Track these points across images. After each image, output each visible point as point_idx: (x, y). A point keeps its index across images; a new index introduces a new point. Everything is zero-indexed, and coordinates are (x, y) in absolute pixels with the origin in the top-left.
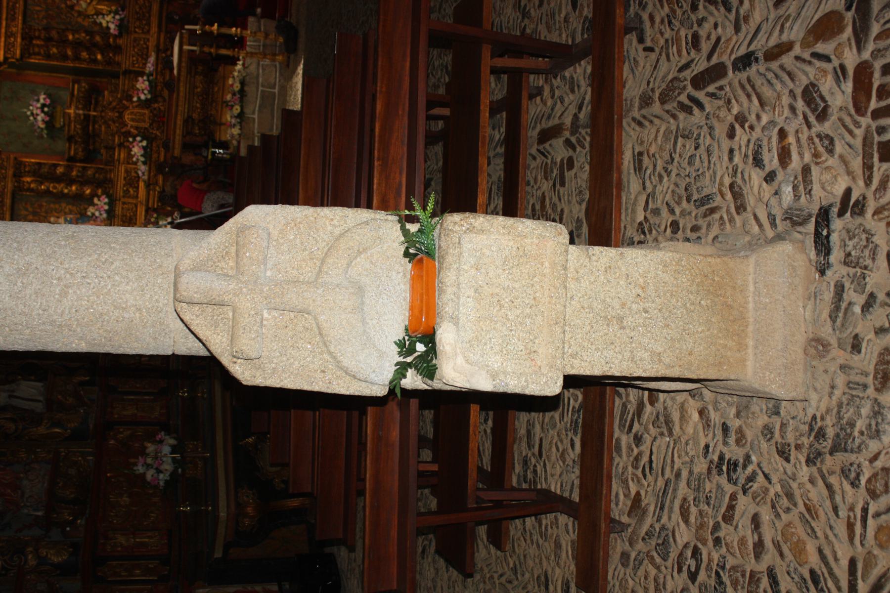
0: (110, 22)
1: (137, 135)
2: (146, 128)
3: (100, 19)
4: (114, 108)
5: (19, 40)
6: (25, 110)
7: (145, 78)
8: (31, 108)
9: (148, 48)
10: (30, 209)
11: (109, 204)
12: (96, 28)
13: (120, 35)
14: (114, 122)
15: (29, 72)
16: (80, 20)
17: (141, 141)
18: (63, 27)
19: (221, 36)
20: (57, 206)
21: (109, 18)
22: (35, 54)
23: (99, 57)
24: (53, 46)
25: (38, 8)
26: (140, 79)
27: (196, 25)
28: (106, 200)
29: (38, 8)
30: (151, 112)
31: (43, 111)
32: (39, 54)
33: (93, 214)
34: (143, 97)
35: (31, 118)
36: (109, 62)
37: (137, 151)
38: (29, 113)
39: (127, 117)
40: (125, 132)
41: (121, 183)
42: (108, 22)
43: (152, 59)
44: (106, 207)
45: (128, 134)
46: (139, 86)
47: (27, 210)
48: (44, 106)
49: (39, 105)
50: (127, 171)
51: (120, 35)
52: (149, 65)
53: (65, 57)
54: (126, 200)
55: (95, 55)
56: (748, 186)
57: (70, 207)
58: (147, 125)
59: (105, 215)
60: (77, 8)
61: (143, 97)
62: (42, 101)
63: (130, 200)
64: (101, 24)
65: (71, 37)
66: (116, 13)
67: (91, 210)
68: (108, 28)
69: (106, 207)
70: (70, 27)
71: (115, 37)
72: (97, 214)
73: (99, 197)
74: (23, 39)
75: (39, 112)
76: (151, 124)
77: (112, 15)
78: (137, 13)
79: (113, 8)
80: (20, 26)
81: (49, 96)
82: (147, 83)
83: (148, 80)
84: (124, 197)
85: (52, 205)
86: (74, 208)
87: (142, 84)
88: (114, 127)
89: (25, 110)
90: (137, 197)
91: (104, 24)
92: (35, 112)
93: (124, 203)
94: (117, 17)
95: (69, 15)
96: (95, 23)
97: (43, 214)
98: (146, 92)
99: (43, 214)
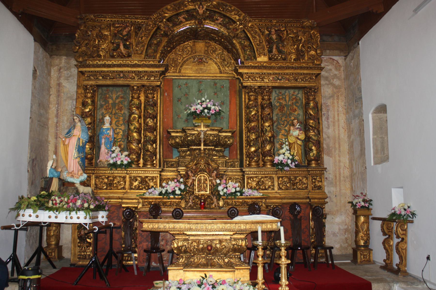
0: (284, 156)
1: (186, 185)
2: (193, 193)
3: (285, 147)
4: (209, 164)
5: (259, 84)
6: (206, 97)
7: (238, 189)
8: (208, 101)
9: (266, 189)
10: (117, 101)
11: (122, 165)
12: (277, 146)
13: (273, 165)
14: (196, 165)
15: (238, 99)
16: (283, 132)
17: (180, 189)
18: (275, 118)
19: (278, 268)
20: (121, 122)
21: (287, 154)
22: (249, 96)
23: (253, 149)
24: (257, 111)
25: (287, 99)
26: (237, 185)
27: (285, 239)
28: (125, 162)
29: (287, 99)
30: (209, 196)
31: (204, 108)
32: (250, 100)
33: (113, 152)
34: (220, 188)
35: (199, 101)
36: (250, 156)
37: (171, 186)
38: (203, 99)
39: (203, 176)
40: (189, 176)
41: (141, 173)
42: (284, 154)
43: (256, 194)
44: (119, 163)
45: (186, 177)
46: (231, 184)
47: (117, 98)
48: (209, 109)
49: (209, 106)
50: (152, 178)
51: (273, 165)
52: (250, 191)
53: (249, 120)
54: (128, 179)
55: (254, 145)
56: (337, 152)
57: (121, 133)
58: (196, 192)
59: (111, 162)
60: (292, 128)
61: (220, 188)
62: (213, 107)
63: (128, 183)
64: (282, 148)
65: (267, 124)
66: (293, 160)
67: (117, 149)
68: (279, 155)
69: (119, 163)
70: (275, 124)
71: (272, 161)
72: (114, 155)
73: (128, 156)
74: (259, 87)
75: (204, 105)
76: (197, 197)
77: (291, 157)
78: (296, 178)
79: (297, 158)
80: (270, 84)
81: (218, 113)
82: (233, 190)
83: (236, 192)
84: (130, 177)
85: (122, 118)
86: (120, 136)
87: (232, 186)
88: (192, 165)
89: (206, 97)
90: (131, 189)
91: (281, 151)
92: (204, 103)
93: (124, 178)
94: (289, 162)
95: (286, 123)
96: (282, 144)
97: (114, 112)
98: (225, 190)
99: (114, 112)
